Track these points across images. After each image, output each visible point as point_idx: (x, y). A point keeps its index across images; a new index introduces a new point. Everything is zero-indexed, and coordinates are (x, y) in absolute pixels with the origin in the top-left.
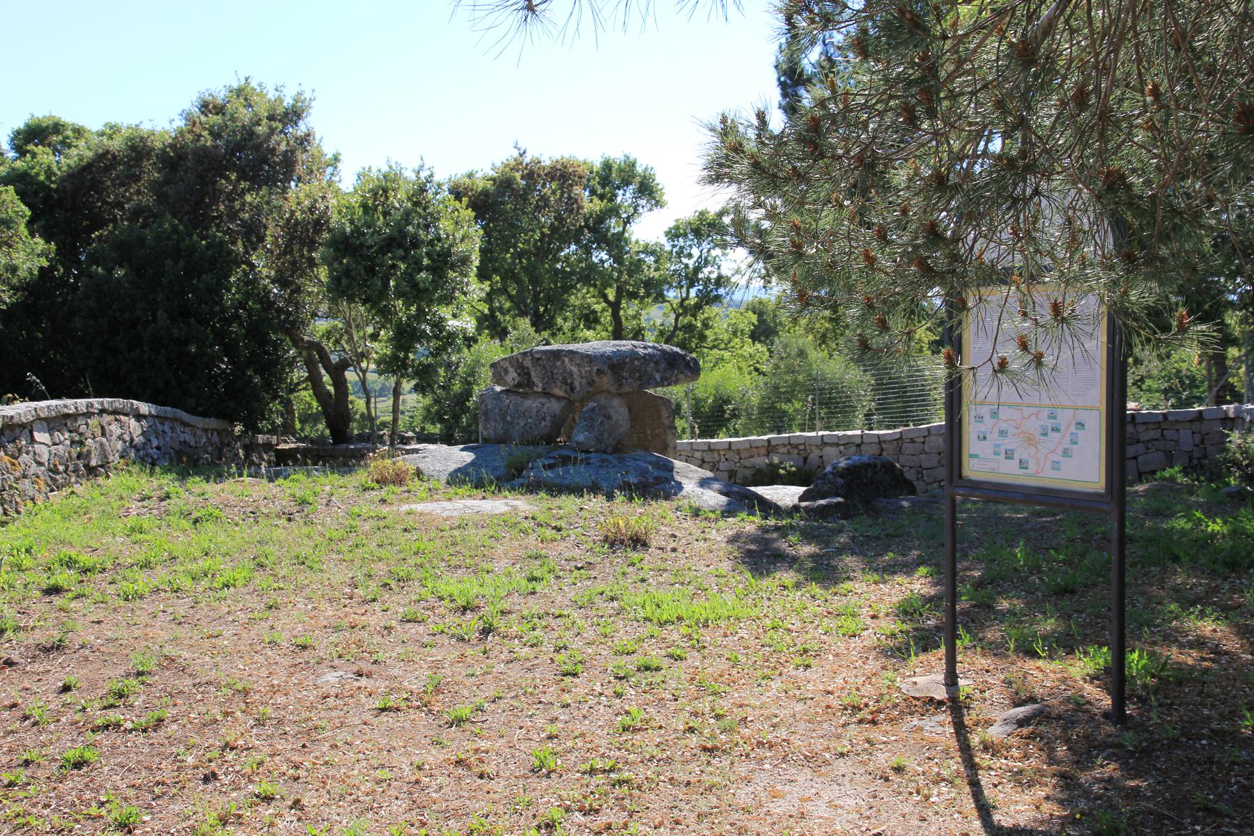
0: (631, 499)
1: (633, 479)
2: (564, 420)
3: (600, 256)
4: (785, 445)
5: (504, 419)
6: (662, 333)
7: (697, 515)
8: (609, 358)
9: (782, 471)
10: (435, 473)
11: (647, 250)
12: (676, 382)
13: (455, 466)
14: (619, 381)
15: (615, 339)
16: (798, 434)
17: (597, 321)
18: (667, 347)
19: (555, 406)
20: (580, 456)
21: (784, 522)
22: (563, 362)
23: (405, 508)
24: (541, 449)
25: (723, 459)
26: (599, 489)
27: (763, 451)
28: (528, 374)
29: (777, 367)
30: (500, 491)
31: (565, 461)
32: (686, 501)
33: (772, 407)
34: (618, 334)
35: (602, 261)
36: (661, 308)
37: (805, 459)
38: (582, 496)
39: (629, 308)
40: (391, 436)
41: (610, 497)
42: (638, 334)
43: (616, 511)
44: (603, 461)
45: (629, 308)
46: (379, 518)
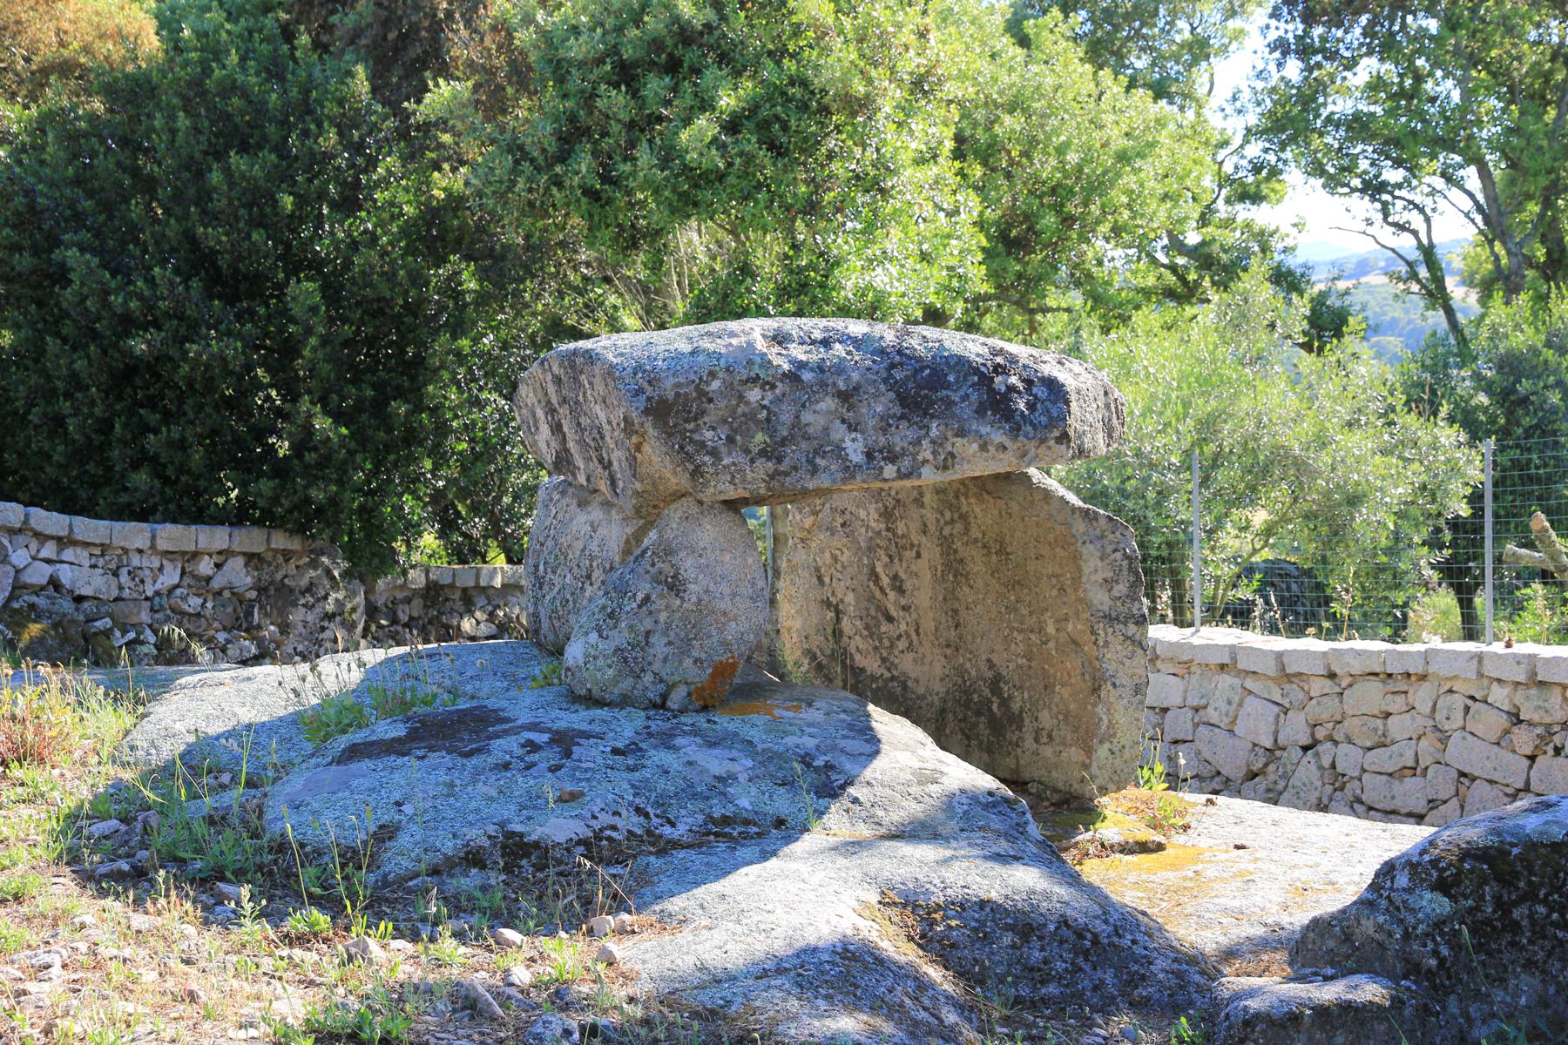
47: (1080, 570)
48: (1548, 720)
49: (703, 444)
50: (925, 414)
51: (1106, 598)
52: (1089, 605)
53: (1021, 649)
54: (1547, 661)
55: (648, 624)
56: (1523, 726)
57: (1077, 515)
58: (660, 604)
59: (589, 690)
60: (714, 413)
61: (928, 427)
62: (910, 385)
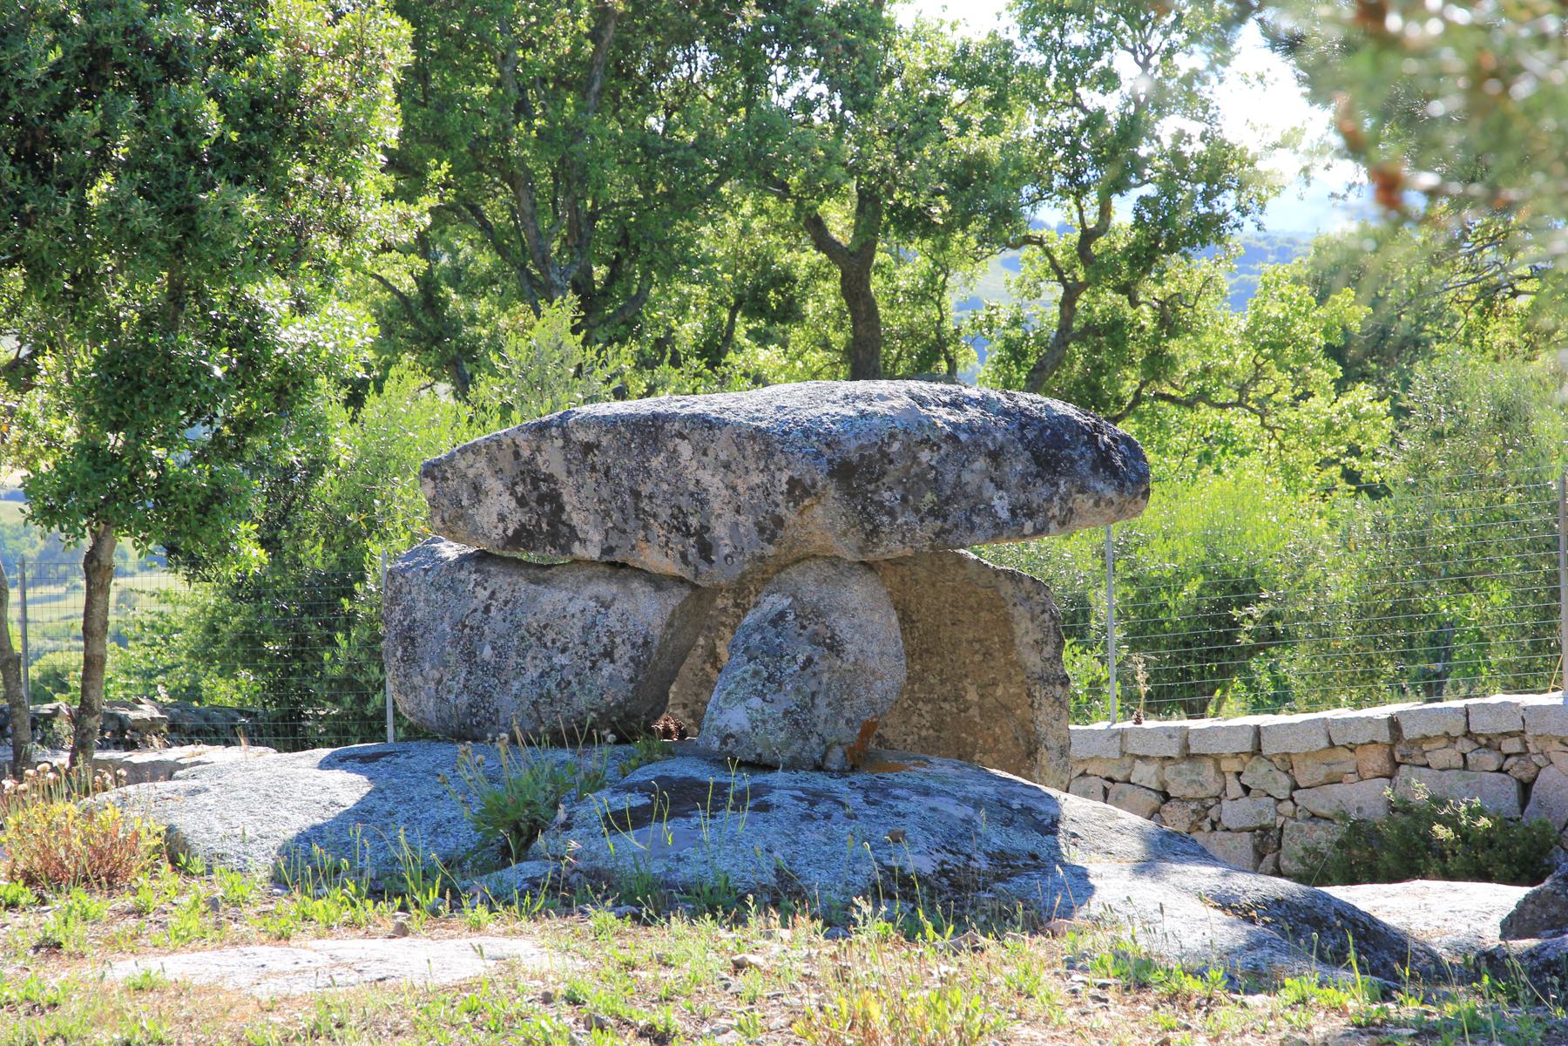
0: (911, 932)
1: (918, 861)
2: (681, 657)
3: (795, 86)
4: (1451, 740)
5: (470, 656)
6: (1015, 351)
7: (1143, 986)
8: (831, 441)
9: (1442, 832)
10: (231, 847)
11: (969, 69)
12: (1066, 522)
13: (302, 821)
14: (868, 521)
15: (854, 376)
16: (1497, 698)
17: (790, 312)
18: (1025, 399)
19: (647, 610)
20: (740, 781)
21: (1449, 1009)
22: (674, 456)
23: (124, 969)
24: (598, 759)
25: (1234, 789)
26: (800, 894)
27: (1376, 760)
28: (554, 498)
29: (1421, 468)
30: (456, 906)
31: (684, 798)
32: (1103, 938)
33: (1404, 609)
34: (863, 360)
35: (807, 106)
36: (1012, 265)
37: (1525, 788)
38: (740, 920)
39: (901, 266)
40: (76, 720)
41: (838, 922)
42: (932, 355)
43: (859, 972)
44: (814, 798)
45: (901, 266)
46: (34, 1008)
47: (1011, 632)
48: (1202, 794)
49: (881, 504)
50: (1055, 472)
51: (1038, 660)
52: (1024, 668)
53: (928, 719)
54: (1201, 732)
55: (813, 686)
56: (1173, 802)
57: (1002, 577)
58: (823, 665)
59: (759, 755)
60: (894, 471)
61: (1057, 485)
62: (1041, 444)
